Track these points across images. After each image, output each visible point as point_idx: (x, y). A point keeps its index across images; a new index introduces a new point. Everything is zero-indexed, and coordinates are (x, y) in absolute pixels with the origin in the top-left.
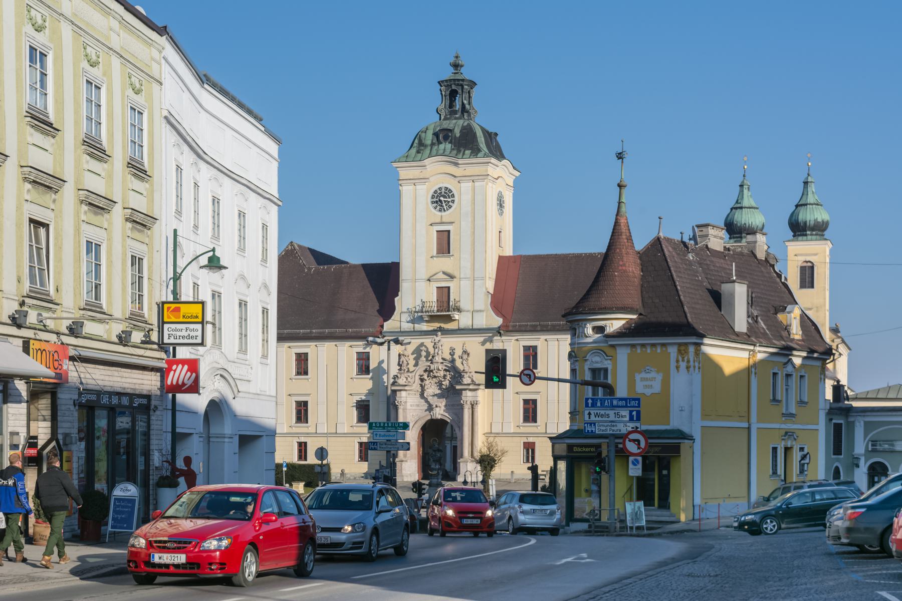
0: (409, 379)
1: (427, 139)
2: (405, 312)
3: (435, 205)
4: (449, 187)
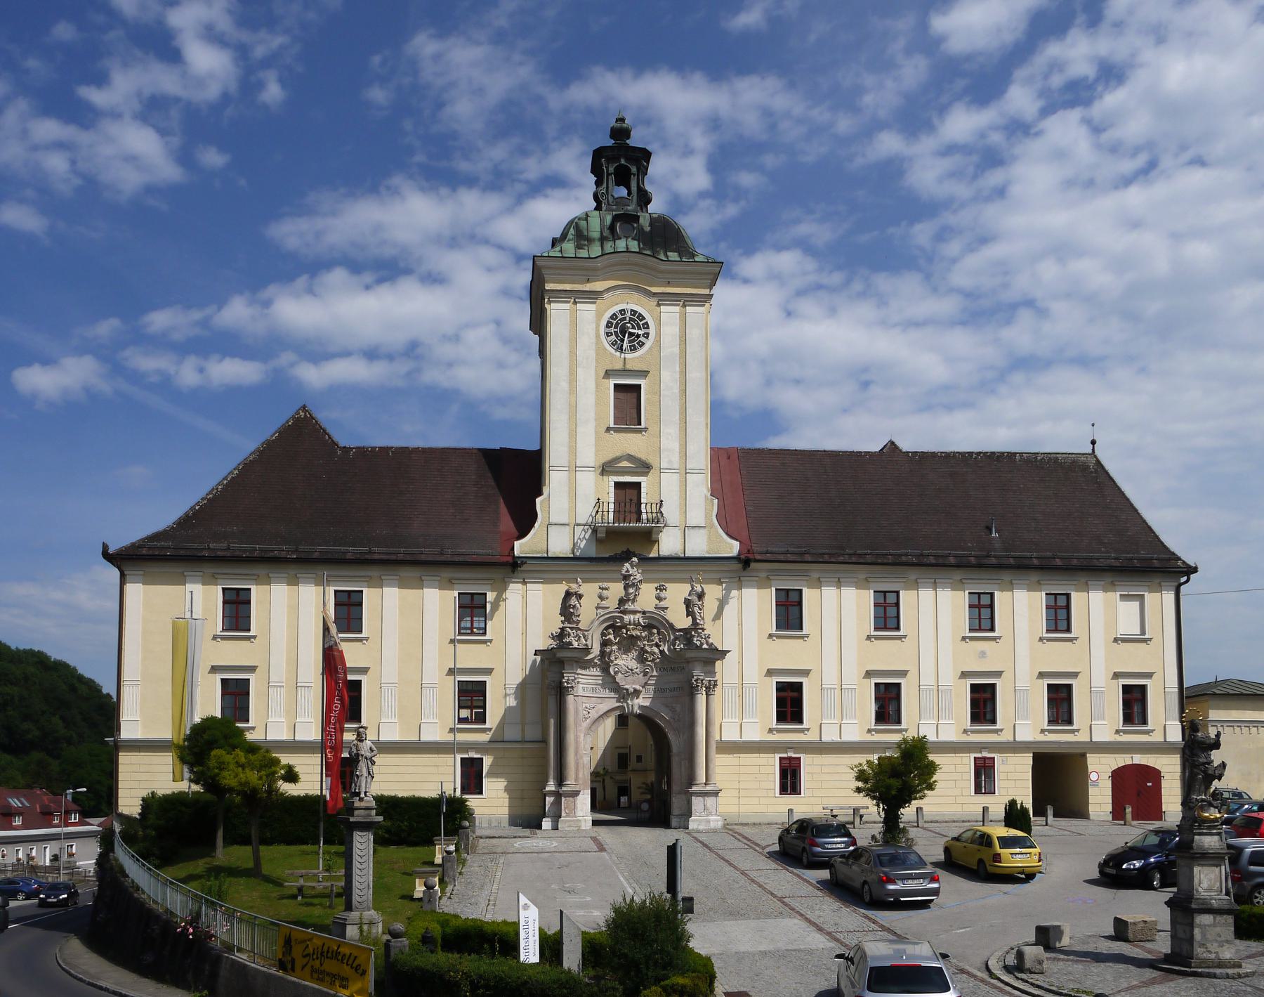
1: (591, 229)
4: (639, 309)
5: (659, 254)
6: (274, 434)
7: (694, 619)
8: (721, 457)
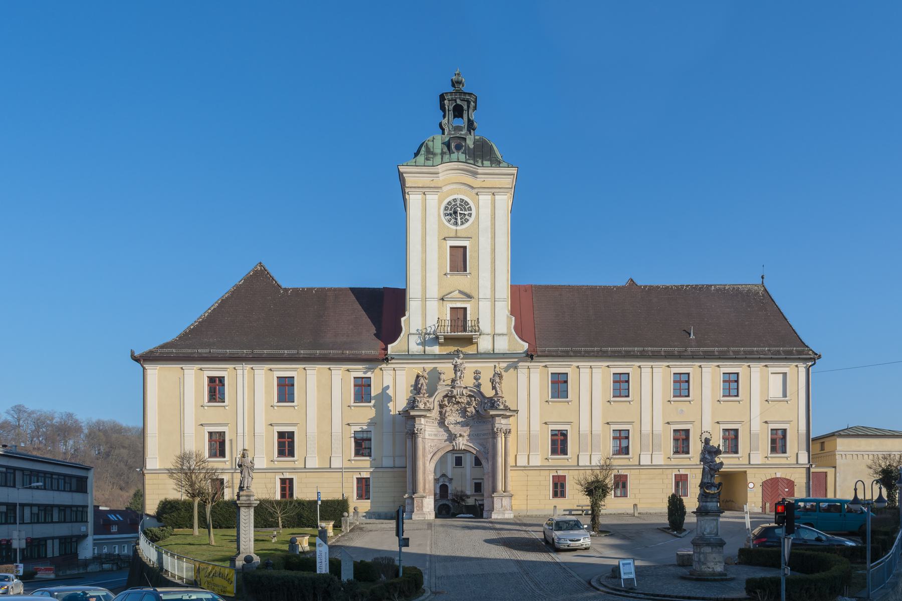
0: (428, 404)
2: (414, 334)
3: (449, 217)
4: (466, 199)
5: (477, 162)
6: (241, 281)
7: (496, 391)
8: (518, 293)
